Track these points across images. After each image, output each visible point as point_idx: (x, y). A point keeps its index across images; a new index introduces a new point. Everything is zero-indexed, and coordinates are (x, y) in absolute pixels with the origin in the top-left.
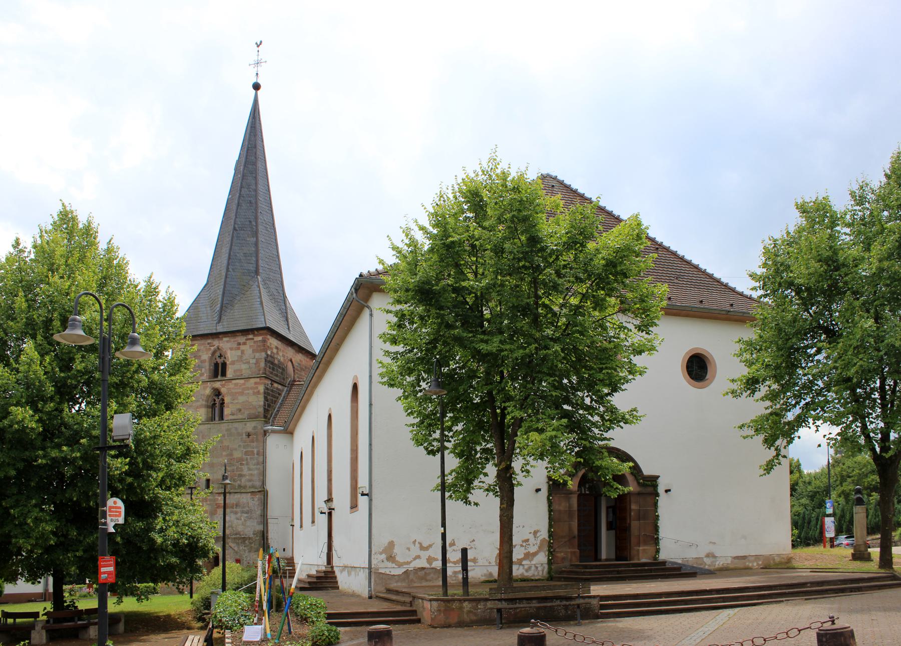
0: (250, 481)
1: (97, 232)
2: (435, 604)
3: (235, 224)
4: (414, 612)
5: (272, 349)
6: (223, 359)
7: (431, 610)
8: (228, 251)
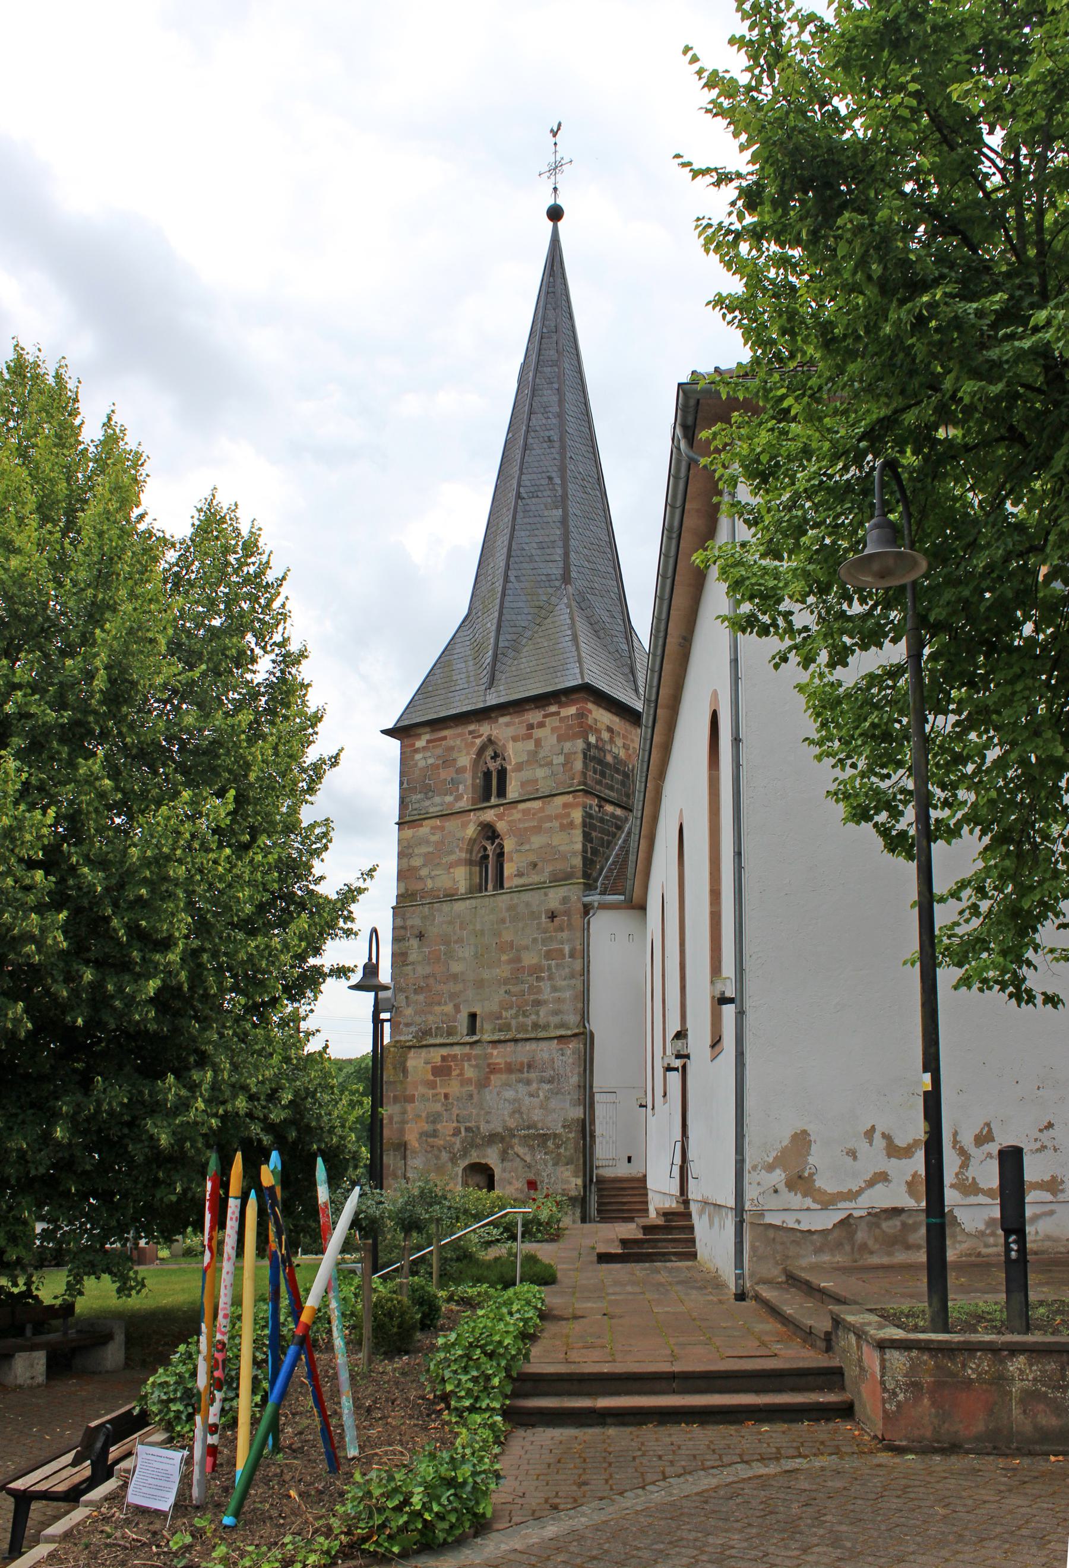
0: (556, 1013)
1: (76, 400)
2: (898, 1359)
3: (519, 485)
4: (833, 1377)
5: (598, 731)
6: (499, 761)
7: (882, 1383)
8: (506, 543)
